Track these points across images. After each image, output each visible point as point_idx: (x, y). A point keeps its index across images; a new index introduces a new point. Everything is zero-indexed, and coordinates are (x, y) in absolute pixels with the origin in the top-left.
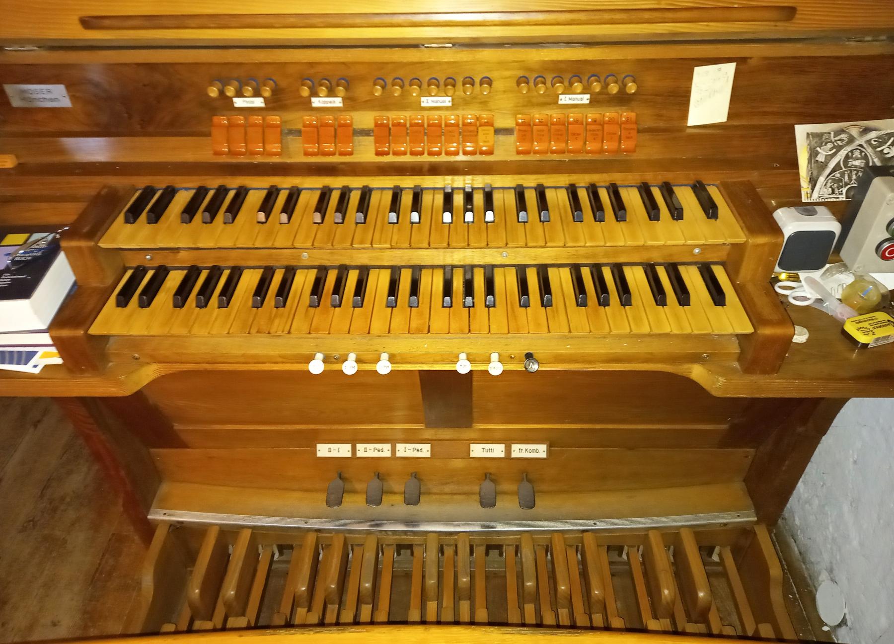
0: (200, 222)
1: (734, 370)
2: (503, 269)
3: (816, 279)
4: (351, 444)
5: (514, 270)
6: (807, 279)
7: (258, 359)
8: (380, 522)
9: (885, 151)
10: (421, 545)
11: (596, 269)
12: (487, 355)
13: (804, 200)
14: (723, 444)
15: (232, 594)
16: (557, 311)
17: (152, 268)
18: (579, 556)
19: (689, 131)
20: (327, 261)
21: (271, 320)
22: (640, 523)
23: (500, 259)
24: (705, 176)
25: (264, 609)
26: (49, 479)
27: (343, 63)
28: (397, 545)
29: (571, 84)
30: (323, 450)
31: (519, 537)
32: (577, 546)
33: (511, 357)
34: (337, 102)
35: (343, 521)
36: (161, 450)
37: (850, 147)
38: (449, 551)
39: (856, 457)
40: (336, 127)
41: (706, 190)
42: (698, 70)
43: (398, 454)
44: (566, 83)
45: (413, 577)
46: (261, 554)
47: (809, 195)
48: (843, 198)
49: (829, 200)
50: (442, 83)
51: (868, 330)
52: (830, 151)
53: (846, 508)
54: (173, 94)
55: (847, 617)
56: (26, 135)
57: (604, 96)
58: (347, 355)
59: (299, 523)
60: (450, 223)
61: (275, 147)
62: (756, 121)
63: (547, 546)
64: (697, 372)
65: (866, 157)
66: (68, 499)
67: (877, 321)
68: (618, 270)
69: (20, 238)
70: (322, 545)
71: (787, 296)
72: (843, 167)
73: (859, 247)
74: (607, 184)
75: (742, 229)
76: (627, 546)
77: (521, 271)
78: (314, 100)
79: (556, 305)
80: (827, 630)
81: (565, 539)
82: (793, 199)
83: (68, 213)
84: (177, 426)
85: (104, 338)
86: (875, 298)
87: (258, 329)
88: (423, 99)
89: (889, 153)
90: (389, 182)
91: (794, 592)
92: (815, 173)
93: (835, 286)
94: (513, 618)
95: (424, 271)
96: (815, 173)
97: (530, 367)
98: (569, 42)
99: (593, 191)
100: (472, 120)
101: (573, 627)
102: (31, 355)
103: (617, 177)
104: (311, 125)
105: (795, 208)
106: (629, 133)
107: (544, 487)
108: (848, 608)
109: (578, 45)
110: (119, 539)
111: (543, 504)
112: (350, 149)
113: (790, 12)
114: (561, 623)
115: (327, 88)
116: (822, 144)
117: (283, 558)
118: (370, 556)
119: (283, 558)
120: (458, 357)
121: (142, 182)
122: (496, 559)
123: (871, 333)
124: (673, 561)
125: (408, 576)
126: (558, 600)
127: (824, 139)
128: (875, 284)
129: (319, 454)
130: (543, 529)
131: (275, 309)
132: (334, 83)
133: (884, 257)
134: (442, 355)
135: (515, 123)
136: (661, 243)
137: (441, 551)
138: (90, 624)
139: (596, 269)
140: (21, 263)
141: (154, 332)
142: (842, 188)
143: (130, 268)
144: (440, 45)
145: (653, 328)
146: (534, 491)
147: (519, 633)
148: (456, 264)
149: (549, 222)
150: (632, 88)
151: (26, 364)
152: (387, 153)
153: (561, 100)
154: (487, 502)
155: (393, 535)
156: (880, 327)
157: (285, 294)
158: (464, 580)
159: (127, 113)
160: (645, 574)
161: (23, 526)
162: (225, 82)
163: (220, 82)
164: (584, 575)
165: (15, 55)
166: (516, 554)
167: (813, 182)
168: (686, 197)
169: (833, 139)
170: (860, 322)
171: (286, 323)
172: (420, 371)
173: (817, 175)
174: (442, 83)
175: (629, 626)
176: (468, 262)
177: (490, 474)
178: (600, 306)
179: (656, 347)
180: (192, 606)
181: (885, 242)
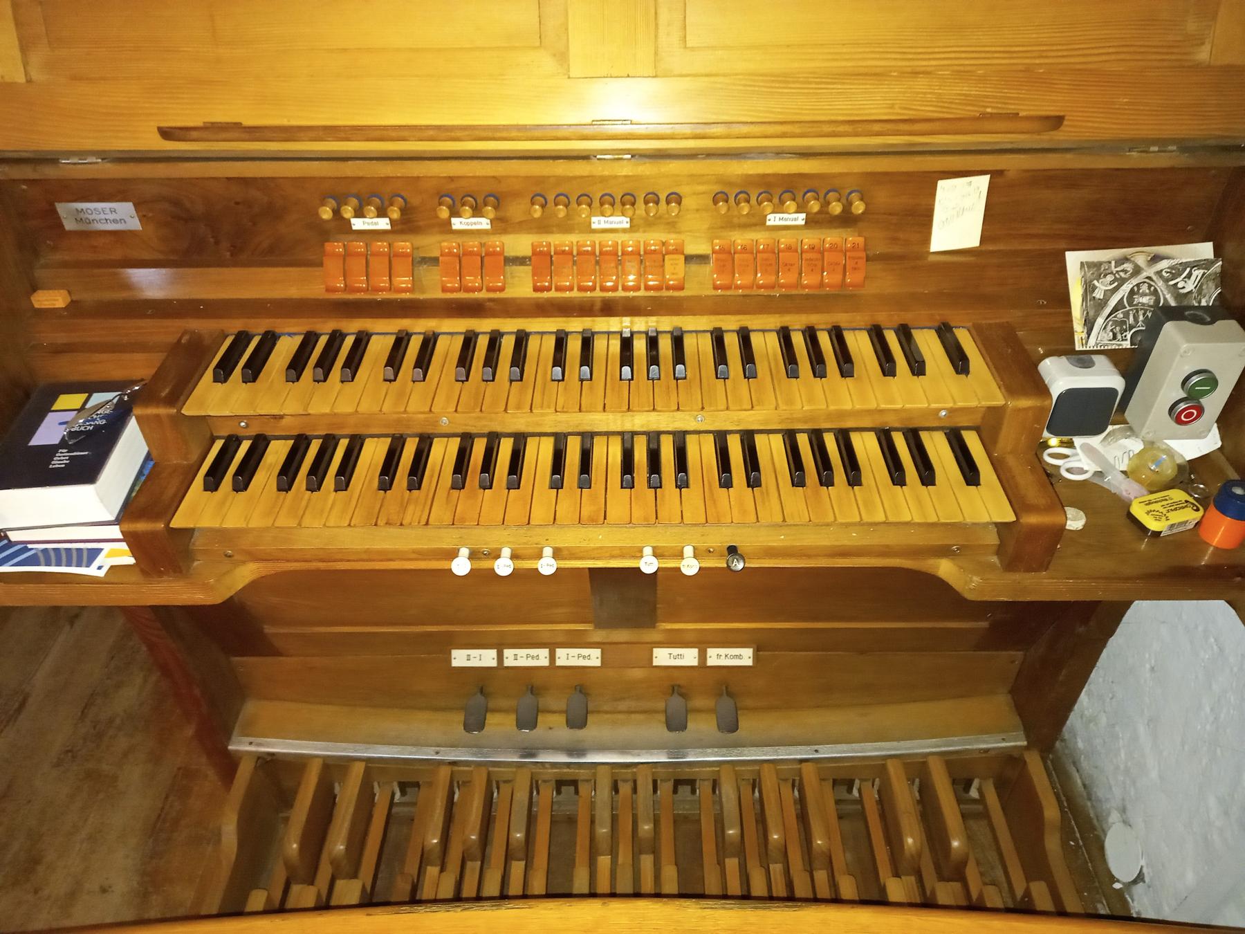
0: (311, 379)
1: (992, 567)
2: (697, 436)
3: (1095, 446)
4: (496, 650)
5: (711, 437)
6: (1082, 446)
7: (386, 556)
8: (534, 751)
9: (1180, 285)
10: (587, 781)
11: (816, 438)
12: (679, 548)
13: (1078, 347)
14: (979, 647)
15: (342, 850)
16: (768, 494)
17: (248, 438)
18: (796, 793)
19: (931, 258)
20: (473, 428)
21: (404, 507)
22: (876, 750)
23: (695, 423)
24: (952, 316)
25: (382, 867)
26: (92, 694)
27: (494, 177)
28: (557, 781)
29: (782, 202)
30: (460, 658)
31: (718, 769)
32: (794, 781)
33: (710, 552)
34: (483, 223)
35: (485, 750)
36: (245, 659)
37: (1136, 279)
38: (625, 789)
39: (1153, 662)
40: (483, 255)
41: (953, 332)
42: (943, 185)
43: (559, 663)
44: (776, 200)
45: (579, 823)
46: (377, 794)
47: (1084, 341)
48: (1127, 344)
49: (1110, 348)
50: (618, 200)
51: (1161, 514)
52: (1111, 284)
53: (1142, 729)
54: (273, 212)
55: (1145, 870)
56: (78, 265)
57: (823, 216)
58: (500, 550)
59: (427, 754)
60: (629, 380)
61: (403, 281)
62: (1016, 245)
63: (754, 781)
64: (945, 569)
65: (1155, 293)
66: (118, 721)
67: (1172, 501)
68: (844, 438)
69: (75, 400)
70: (458, 782)
71: (1058, 467)
72: (1127, 305)
73: (1148, 408)
74: (829, 327)
75: (999, 388)
76: (859, 779)
77: (721, 438)
78: (454, 220)
79: (767, 484)
80: (1118, 888)
81: (778, 772)
82: (1064, 346)
83: (141, 367)
84: (268, 629)
85: (188, 533)
86: (1169, 472)
87: (388, 519)
88: (594, 219)
89: (1184, 288)
90: (552, 324)
91: (1077, 838)
92: (1092, 313)
93: (1119, 454)
94: (712, 886)
95: (596, 439)
96: (1092, 313)
97: (734, 565)
98: (779, 153)
99: (811, 335)
100: (657, 247)
101: (790, 899)
102: (94, 553)
103: (841, 319)
104: (450, 254)
105: (1067, 359)
106: (857, 263)
107: (749, 702)
108: (1145, 859)
109: (791, 155)
110: (188, 774)
111: (748, 724)
112: (500, 284)
113: (1057, 122)
114: (775, 895)
115: (471, 207)
116: (1100, 276)
117: (406, 799)
118: (522, 796)
119: (406, 799)
120: (641, 551)
121: (234, 326)
122: (689, 799)
123: (1164, 518)
124: (918, 798)
125: (571, 821)
126: (769, 853)
127: (1102, 269)
128: (1170, 453)
129: (455, 663)
130: (749, 758)
131: (408, 492)
132: (480, 201)
133: (1179, 421)
134: (621, 548)
135: (711, 249)
136: (899, 406)
137: (615, 788)
138: (151, 889)
139: (816, 438)
140: (81, 436)
141: (253, 524)
142: (1126, 331)
143: (220, 438)
144: (616, 157)
145: (888, 514)
146: (736, 707)
147: (723, 908)
148: (639, 430)
149: (755, 378)
150: (859, 207)
151: (88, 565)
152: (548, 289)
153: (769, 220)
154: (676, 724)
155: (552, 768)
156: (1176, 509)
157: (420, 473)
158: (646, 827)
159: (213, 237)
160: (883, 816)
161: (59, 758)
162: (341, 200)
163: (334, 200)
164: (803, 817)
165: (70, 169)
166: (714, 791)
167: (1089, 324)
168: (929, 344)
169: (1114, 270)
170: (1150, 503)
171: (422, 511)
172: (590, 569)
173: (1094, 316)
174: (618, 200)
175: (865, 897)
176: (653, 427)
177: (679, 686)
178: (821, 485)
179: (891, 538)
180: (288, 866)
181: (1182, 402)
